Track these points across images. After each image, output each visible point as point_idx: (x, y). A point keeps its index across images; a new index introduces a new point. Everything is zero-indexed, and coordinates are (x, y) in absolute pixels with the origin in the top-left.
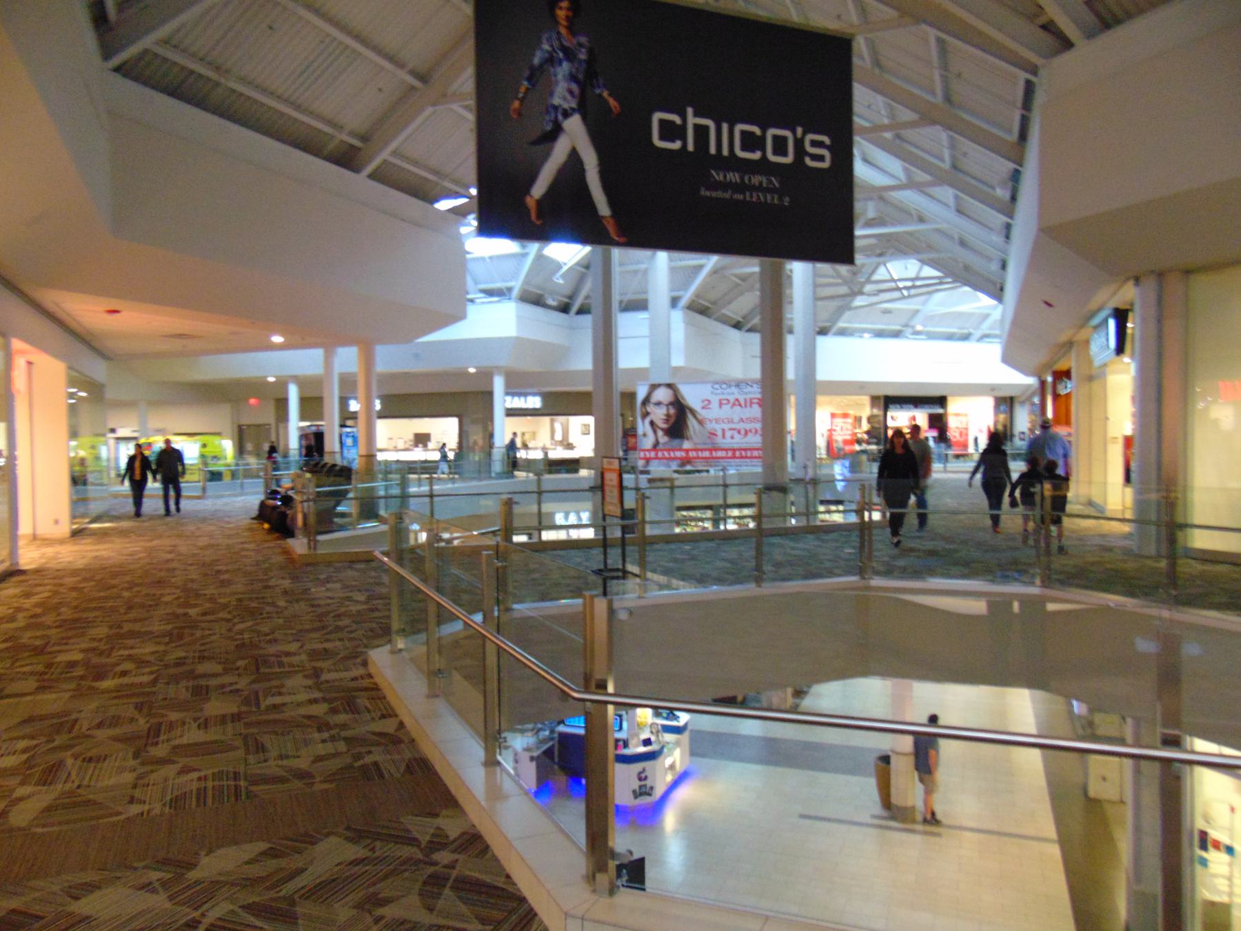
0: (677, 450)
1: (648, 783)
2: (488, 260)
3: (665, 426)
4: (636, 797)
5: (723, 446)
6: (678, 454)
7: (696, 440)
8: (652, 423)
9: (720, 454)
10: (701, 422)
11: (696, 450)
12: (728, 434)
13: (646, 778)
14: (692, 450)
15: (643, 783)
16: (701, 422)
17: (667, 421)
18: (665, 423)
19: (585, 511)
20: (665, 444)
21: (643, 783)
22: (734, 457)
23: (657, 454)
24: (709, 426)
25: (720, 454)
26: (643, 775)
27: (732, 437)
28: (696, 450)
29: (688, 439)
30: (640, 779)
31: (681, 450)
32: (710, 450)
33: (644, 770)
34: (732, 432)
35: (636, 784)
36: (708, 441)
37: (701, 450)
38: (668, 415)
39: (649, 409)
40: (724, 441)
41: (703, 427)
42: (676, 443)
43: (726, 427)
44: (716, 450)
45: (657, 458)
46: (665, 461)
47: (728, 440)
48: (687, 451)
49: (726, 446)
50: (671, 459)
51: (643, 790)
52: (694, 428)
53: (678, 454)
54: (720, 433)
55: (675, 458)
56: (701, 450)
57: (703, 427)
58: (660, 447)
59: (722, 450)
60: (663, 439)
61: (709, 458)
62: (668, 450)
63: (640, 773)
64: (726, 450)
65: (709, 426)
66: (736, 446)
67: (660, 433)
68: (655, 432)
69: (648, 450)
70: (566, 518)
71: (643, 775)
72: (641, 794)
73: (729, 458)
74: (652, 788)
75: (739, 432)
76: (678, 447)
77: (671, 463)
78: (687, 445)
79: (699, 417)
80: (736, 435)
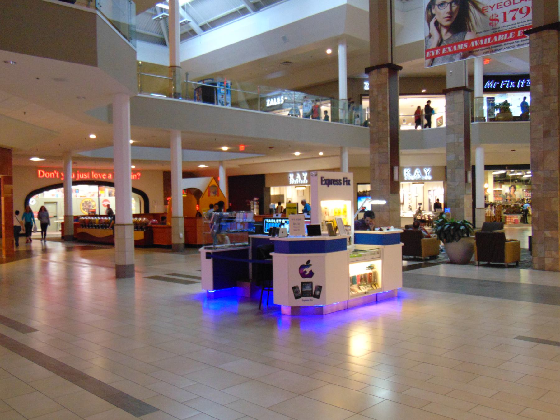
0: (460, 43)
1: (315, 281)
2: (497, 191)
3: (448, 23)
4: (297, 298)
5: (504, 29)
6: (460, 47)
7: (477, 29)
8: (437, 24)
9: (501, 38)
10: (482, 12)
11: (478, 39)
12: (509, 16)
13: (311, 274)
14: (473, 40)
15: (307, 280)
16: (482, 12)
17: (450, 18)
18: (448, 21)
19: (427, 167)
20: (449, 39)
21: (307, 280)
22: (516, 37)
23: (441, 51)
24: (490, 13)
25: (501, 38)
26: (308, 270)
27: (514, 19)
28: (478, 39)
29: (470, 31)
30: (303, 275)
31: (464, 42)
32: (492, 36)
33: (308, 264)
34: (512, 14)
35: (298, 280)
36: (490, 27)
37: (483, 38)
38: (451, 13)
39: (434, 12)
40: (506, 24)
41: (484, 15)
42: (458, 37)
43: (507, 9)
44: (497, 35)
45: (441, 54)
46: (449, 56)
47: (509, 21)
48: (469, 42)
49: (508, 29)
50: (455, 53)
51: (308, 288)
52: (475, 17)
53: (460, 47)
54: (501, 18)
55: (458, 51)
56: (483, 38)
57: (484, 15)
58: (444, 43)
59: (504, 33)
60: (446, 35)
61: (490, 44)
62: (452, 45)
63: (302, 267)
64: (508, 32)
65: (490, 13)
66: (517, 26)
67: (444, 31)
68: (439, 31)
69: (434, 49)
70: (412, 173)
71: (308, 270)
72: (305, 294)
73: (512, 39)
74: (319, 288)
75: (521, 12)
76: (460, 40)
77: (454, 57)
78: (469, 36)
79: (481, 7)
80: (518, 15)
